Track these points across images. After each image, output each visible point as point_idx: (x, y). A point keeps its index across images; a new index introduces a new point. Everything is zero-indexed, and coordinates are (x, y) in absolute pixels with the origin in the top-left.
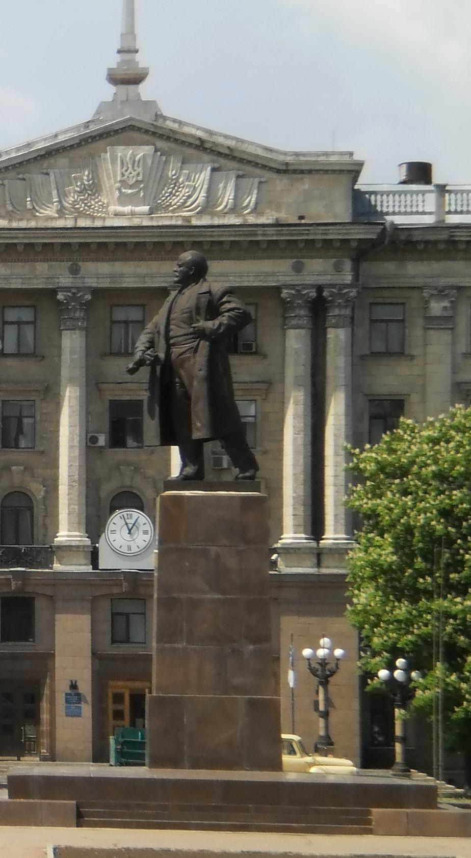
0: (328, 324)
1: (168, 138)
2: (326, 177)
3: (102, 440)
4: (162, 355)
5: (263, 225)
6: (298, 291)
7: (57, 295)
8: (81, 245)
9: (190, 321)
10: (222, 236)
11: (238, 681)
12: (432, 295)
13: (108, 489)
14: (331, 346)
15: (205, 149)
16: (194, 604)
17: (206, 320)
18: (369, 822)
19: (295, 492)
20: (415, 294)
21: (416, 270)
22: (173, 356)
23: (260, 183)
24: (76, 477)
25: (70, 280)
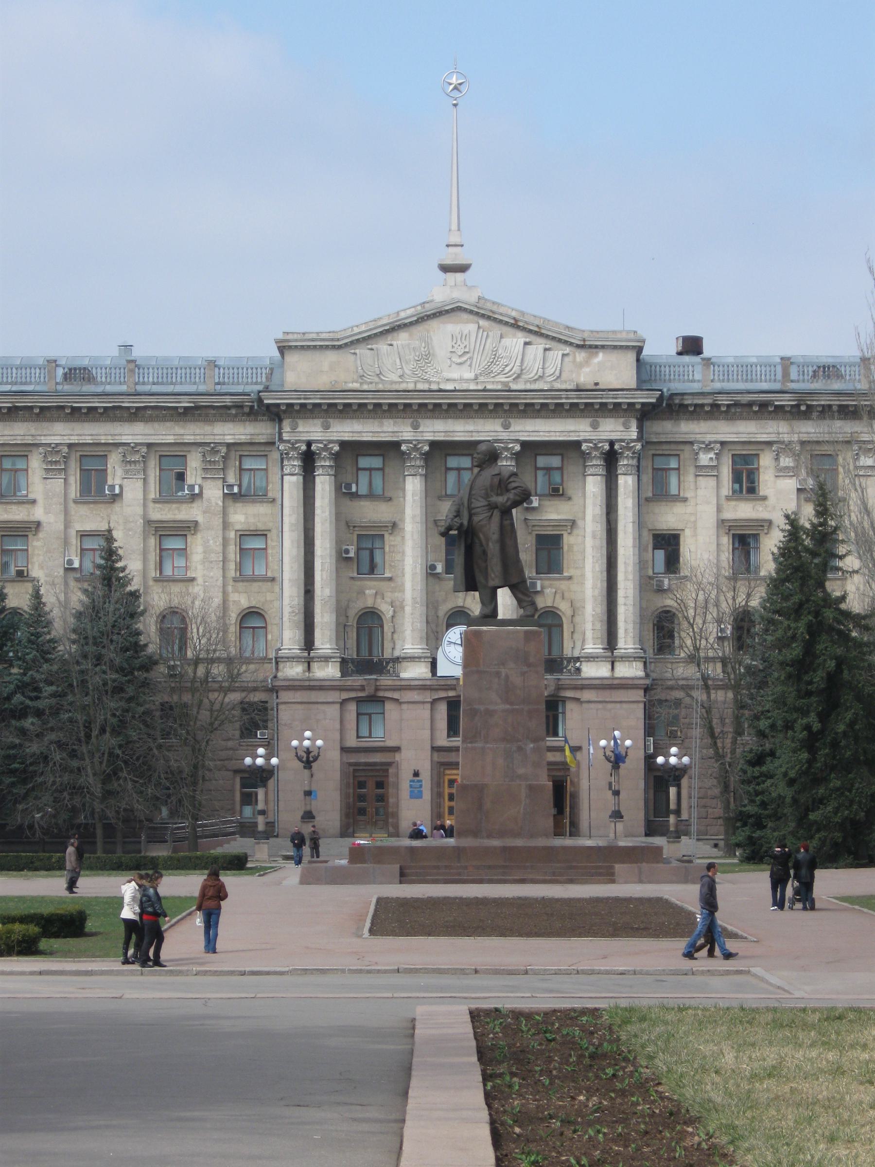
0: (619, 472)
1: (489, 318)
2: (616, 351)
3: (440, 568)
4: (465, 523)
5: (567, 390)
6: (595, 444)
7: (400, 446)
8: (420, 405)
9: (487, 496)
10: (533, 398)
11: (521, 771)
12: (700, 448)
13: (444, 609)
14: (621, 490)
15: (518, 327)
16: (489, 713)
17: (498, 495)
18: (613, 874)
19: (594, 611)
20: (687, 448)
21: (689, 429)
22: (474, 523)
23: (563, 355)
24: (419, 600)
25: (412, 434)
